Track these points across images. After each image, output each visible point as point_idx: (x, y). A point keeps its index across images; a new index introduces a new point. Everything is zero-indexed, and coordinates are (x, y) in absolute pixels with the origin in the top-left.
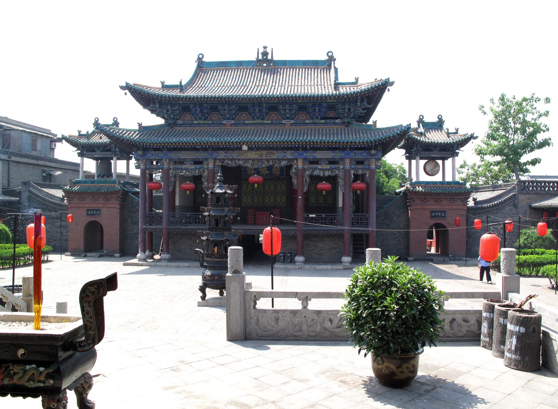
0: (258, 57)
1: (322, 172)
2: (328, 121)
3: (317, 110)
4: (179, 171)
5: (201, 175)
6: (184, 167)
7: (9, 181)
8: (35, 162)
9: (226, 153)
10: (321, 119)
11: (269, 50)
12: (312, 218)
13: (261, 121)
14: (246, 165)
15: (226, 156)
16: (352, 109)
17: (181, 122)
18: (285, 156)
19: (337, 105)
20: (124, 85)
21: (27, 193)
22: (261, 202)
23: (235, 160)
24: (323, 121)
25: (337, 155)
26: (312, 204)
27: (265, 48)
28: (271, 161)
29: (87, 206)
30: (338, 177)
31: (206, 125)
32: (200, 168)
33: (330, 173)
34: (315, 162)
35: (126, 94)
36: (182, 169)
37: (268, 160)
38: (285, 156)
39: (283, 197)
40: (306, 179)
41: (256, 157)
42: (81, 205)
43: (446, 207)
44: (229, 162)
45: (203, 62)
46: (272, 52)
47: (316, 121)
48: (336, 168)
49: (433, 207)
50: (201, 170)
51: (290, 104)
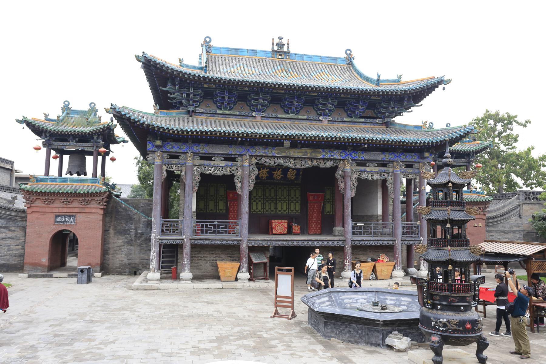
0: (273, 47)
1: (370, 175)
2: (368, 120)
3: (227, 99)
4: (206, 168)
5: (233, 174)
6: (212, 163)
9: (264, 149)
11: (284, 41)
12: (361, 226)
13: (296, 116)
14: (287, 164)
15: (264, 153)
17: (202, 111)
18: (332, 156)
19: (318, 99)
22: (285, 209)
24: (362, 120)
25: (387, 157)
26: (201, 209)
27: (281, 38)
28: (315, 161)
29: (56, 210)
31: (232, 116)
32: (232, 166)
33: (379, 176)
36: (209, 166)
37: (311, 159)
38: (332, 156)
39: (297, 204)
41: (300, 155)
42: (47, 210)
44: (268, 160)
46: (288, 44)
50: (233, 168)
51: (230, 92)
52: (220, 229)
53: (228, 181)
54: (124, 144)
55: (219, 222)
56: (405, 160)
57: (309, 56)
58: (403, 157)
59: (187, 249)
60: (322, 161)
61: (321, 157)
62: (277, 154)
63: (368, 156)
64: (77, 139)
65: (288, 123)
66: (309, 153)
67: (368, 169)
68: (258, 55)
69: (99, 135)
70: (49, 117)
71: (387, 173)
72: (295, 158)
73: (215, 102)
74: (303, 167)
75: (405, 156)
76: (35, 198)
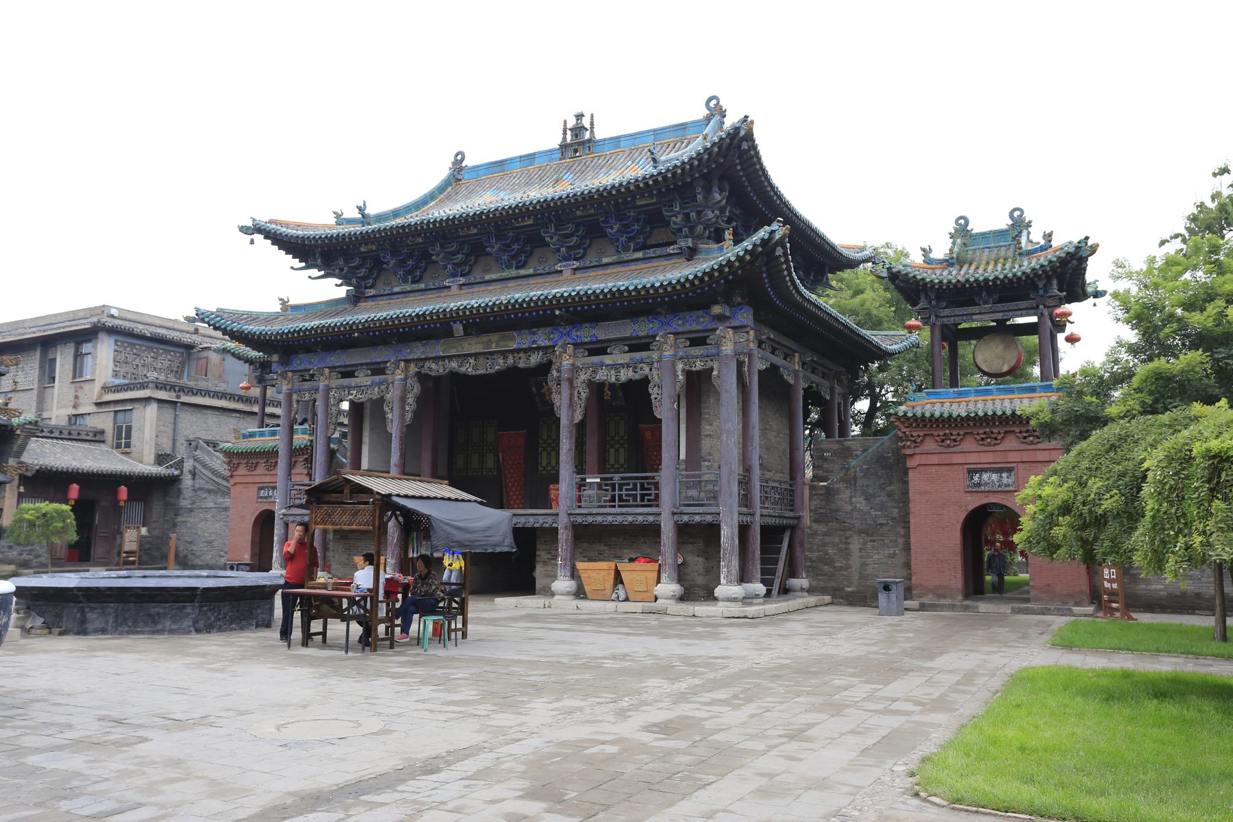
0: (565, 138)
1: (613, 372)
7: (174, 440)
8: (240, 406)
9: (424, 345)
10: (635, 250)
11: (586, 122)
13: (514, 273)
14: (463, 369)
16: (693, 215)
20: (250, 224)
21: (191, 461)
23: (443, 358)
24: (639, 255)
25: (641, 328)
28: (511, 357)
30: (649, 382)
34: (598, 349)
35: (252, 242)
36: (349, 388)
37: (504, 354)
38: (534, 342)
40: (579, 393)
41: (478, 348)
42: (250, 479)
43: (1013, 457)
44: (433, 366)
45: (461, 169)
47: (625, 256)
48: (642, 361)
49: (972, 458)
50: (383, 387)
52: (624, 492)
53: (638, 391)
54: (1096, 300)
55: (623, 479)
56: (680, 330)
57: (631, 135)
58: (677, 324)
59: (564, 536)
60: (522, 355)
61: (515, 346)
62: (444, 351)
63: (602, 332)
64: (996, 296)
65: (418, 297)
66: (494, 342)
67: (608, 360)
68: (622, 144)
69: (1049, 279)
70: (932, 256)
71: (647, 364)
72: (476, 355)
73: (614, 241)
74: (490, 371)
75: (683, 319)
76: (962, 433)
